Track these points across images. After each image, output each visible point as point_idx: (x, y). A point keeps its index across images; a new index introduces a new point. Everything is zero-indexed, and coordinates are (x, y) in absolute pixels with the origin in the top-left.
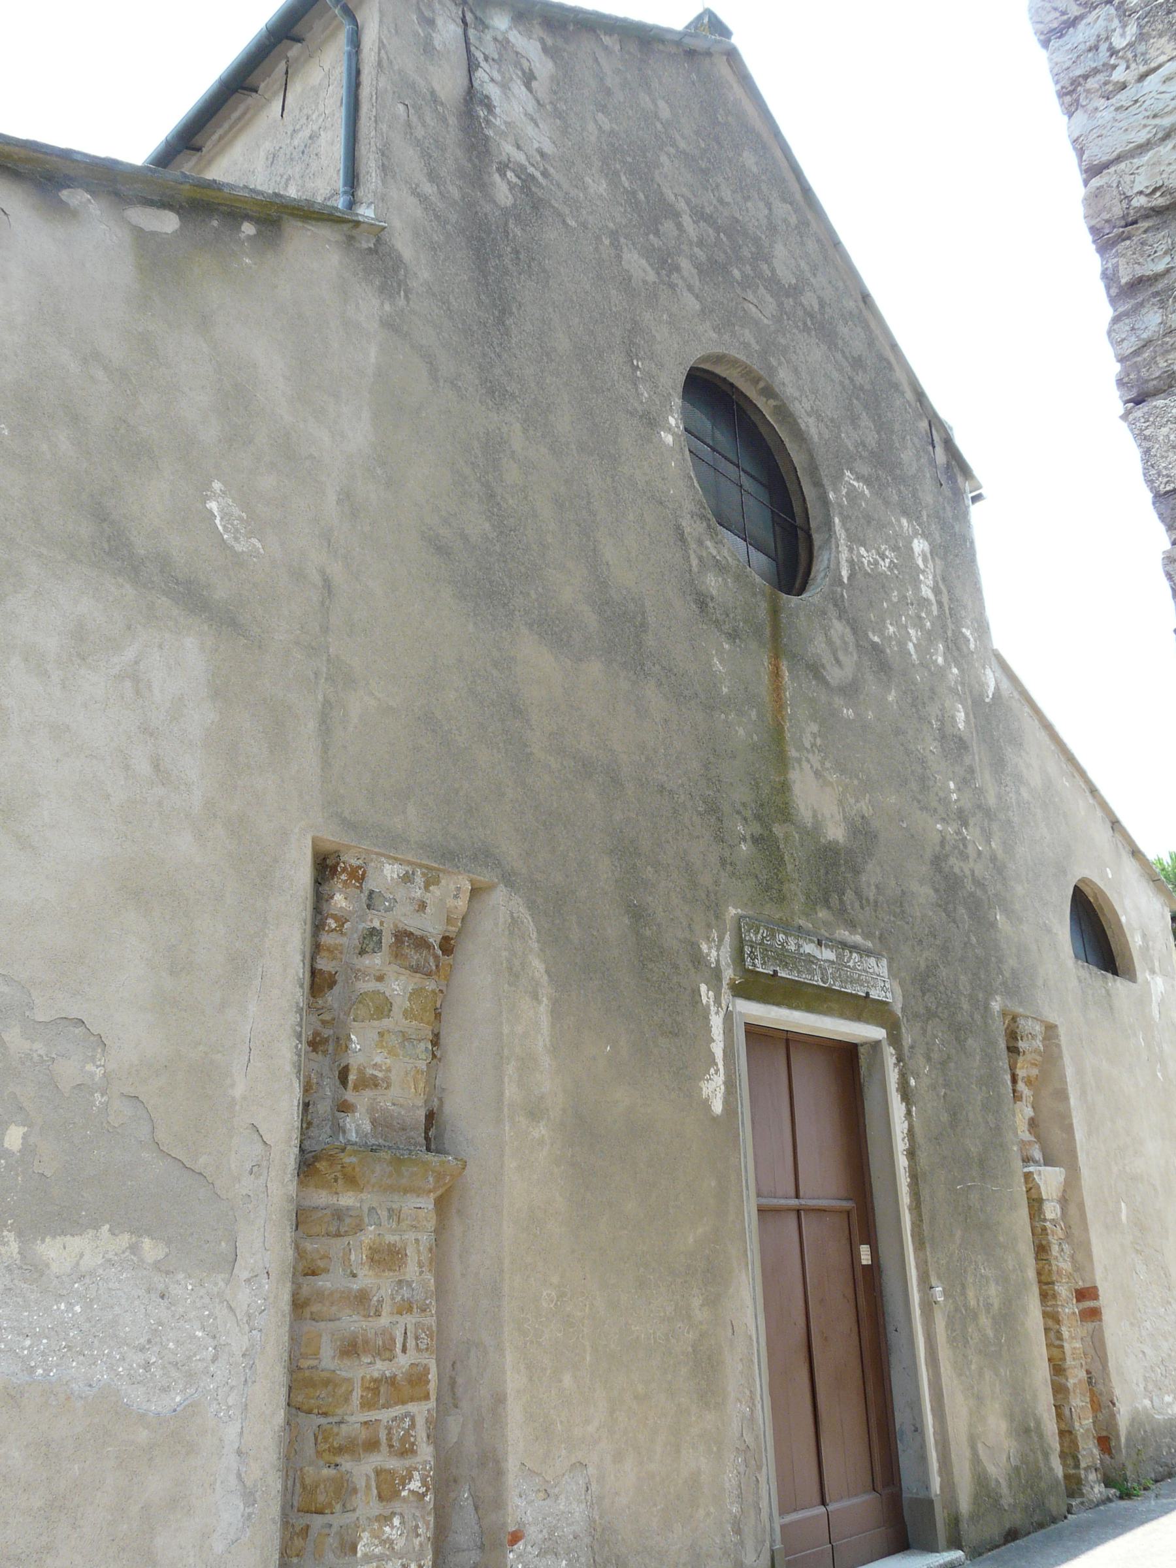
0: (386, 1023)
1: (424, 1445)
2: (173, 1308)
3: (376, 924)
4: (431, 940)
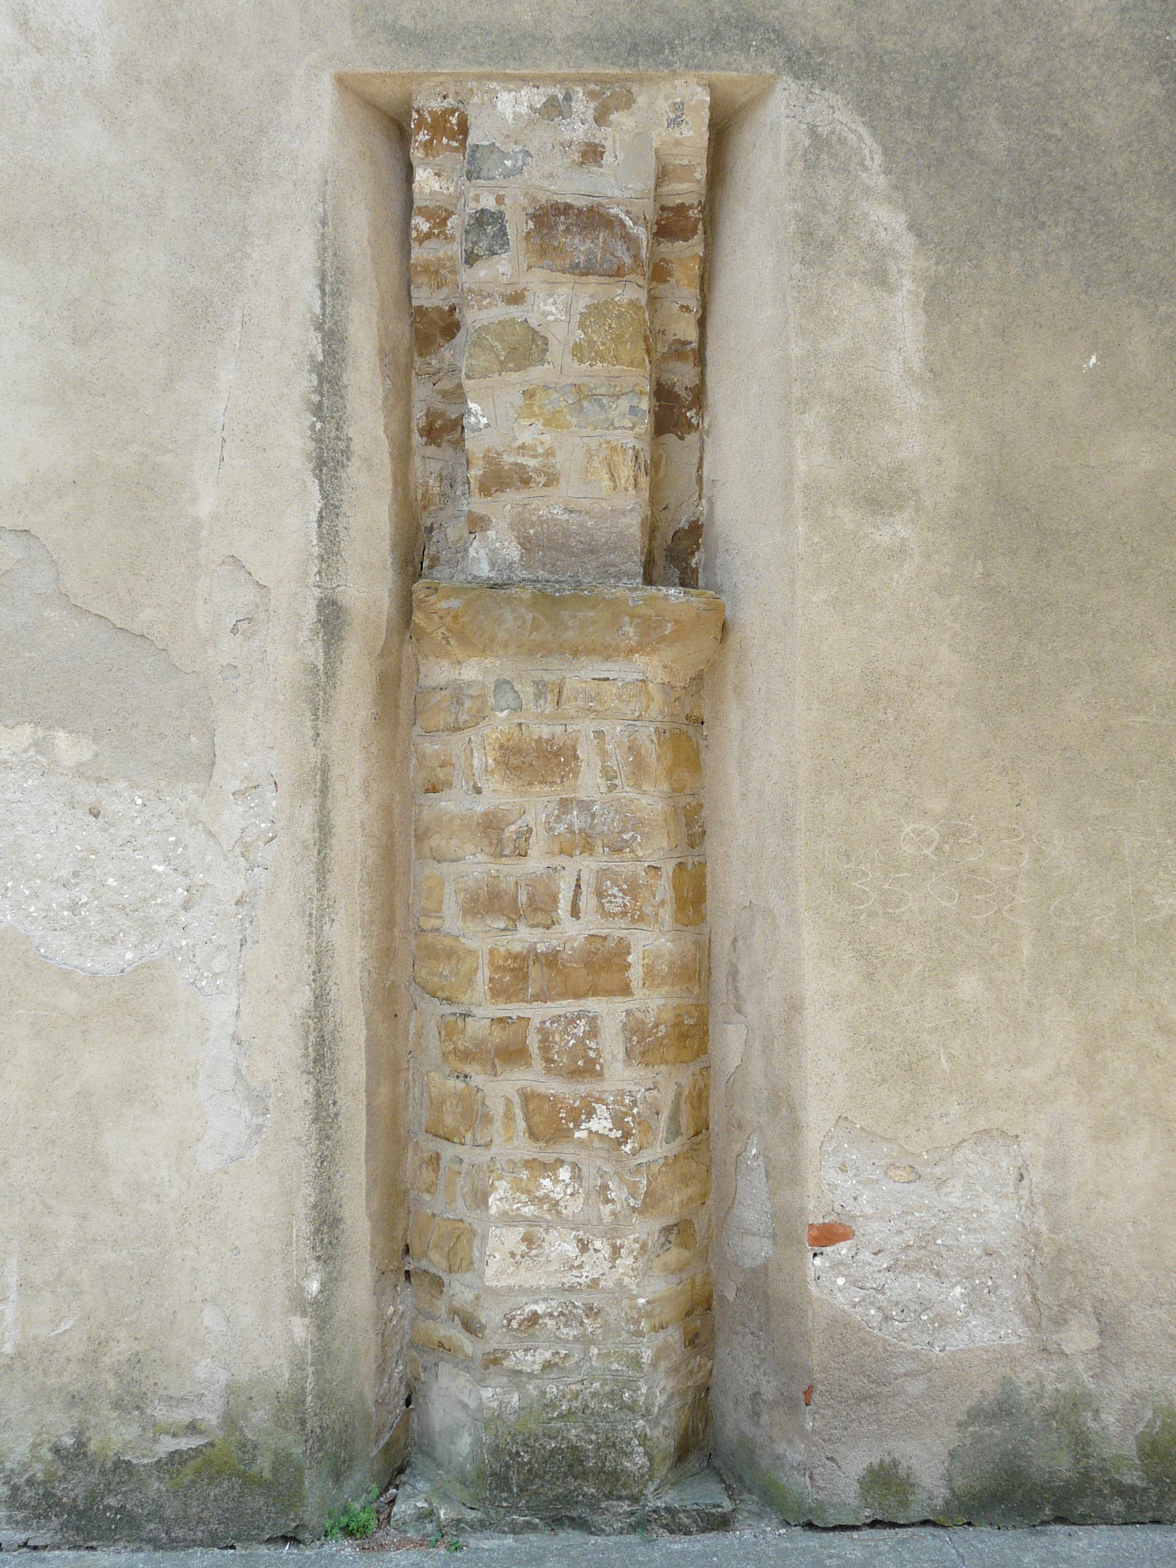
0: (536, 374)
1: (620, 1066)
2: (112, 831)
3: (488, 202)
4: (614, 211)
